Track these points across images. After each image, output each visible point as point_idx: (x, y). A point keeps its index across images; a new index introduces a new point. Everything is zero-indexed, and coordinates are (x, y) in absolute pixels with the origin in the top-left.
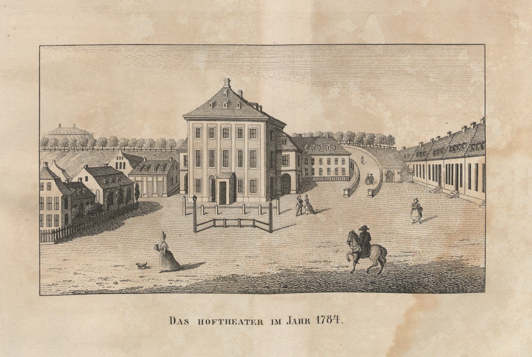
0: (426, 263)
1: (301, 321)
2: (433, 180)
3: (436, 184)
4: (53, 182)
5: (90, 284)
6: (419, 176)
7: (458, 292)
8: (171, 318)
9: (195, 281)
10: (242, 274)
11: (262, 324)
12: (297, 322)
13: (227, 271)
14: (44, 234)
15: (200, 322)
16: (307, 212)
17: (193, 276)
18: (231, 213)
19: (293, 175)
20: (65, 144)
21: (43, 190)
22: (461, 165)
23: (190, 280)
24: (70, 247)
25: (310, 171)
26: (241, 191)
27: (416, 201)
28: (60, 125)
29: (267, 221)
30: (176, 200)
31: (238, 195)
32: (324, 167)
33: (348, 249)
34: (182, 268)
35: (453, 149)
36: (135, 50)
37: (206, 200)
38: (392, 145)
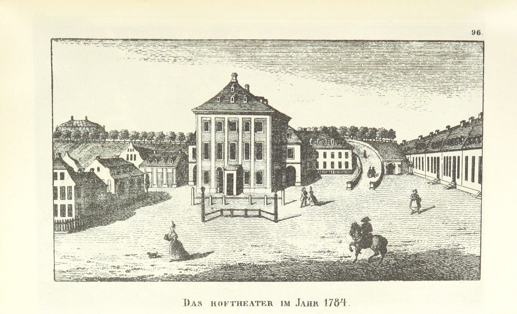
0: (424, 251)
1: (310, 304)
2: (432, 172)
3: (435, 176)
4: (66, 172)
5: (104, 271)
6: (418, 167)
7: (454, 279)
8: (185, 300)
9: (204, 270)
10: (248, 263)
11: (272, 305)
12: (306, 304)
13: (235, 259)
14: (58, 223)
15: (213, 304)
16: (311, 204)
17: (202, 265)
18: (239, 204)
19: (298, 168)
20: (78, 136)
21: (57, 179)
22: (459, 157)
23: (199, 269)
24: (83, 237)
25: (314, 164)
26: (247, 182)
27: (415, 192)
28: (72, 117)
29: (273, 211)
30: (185, 191)
31: (245, 186)
32: (329, 160)
33: (351, 239)
34: (193, 257)
35: (451, 142)
36: (145, 45)
37: (214, 191)
38: (393, 139)
